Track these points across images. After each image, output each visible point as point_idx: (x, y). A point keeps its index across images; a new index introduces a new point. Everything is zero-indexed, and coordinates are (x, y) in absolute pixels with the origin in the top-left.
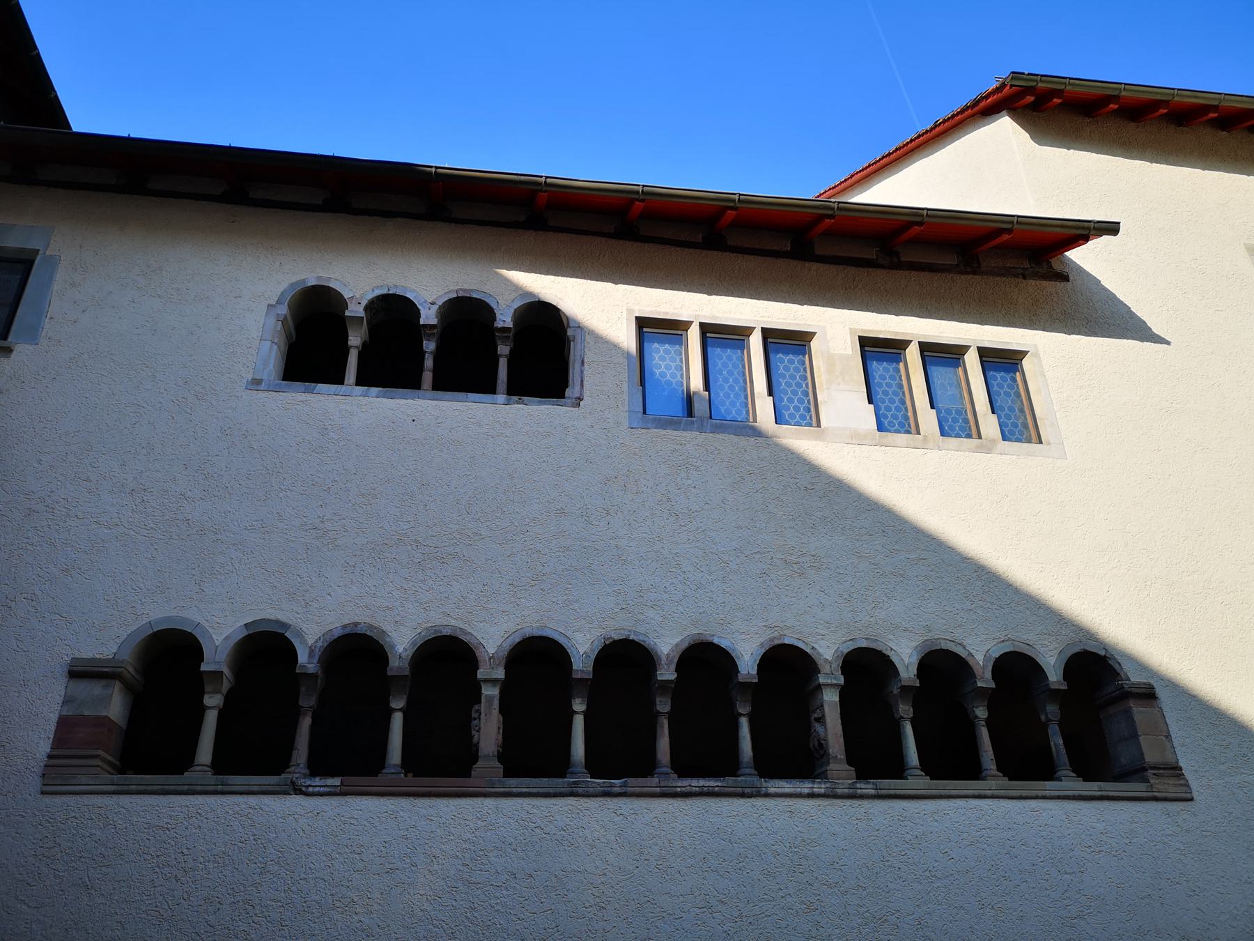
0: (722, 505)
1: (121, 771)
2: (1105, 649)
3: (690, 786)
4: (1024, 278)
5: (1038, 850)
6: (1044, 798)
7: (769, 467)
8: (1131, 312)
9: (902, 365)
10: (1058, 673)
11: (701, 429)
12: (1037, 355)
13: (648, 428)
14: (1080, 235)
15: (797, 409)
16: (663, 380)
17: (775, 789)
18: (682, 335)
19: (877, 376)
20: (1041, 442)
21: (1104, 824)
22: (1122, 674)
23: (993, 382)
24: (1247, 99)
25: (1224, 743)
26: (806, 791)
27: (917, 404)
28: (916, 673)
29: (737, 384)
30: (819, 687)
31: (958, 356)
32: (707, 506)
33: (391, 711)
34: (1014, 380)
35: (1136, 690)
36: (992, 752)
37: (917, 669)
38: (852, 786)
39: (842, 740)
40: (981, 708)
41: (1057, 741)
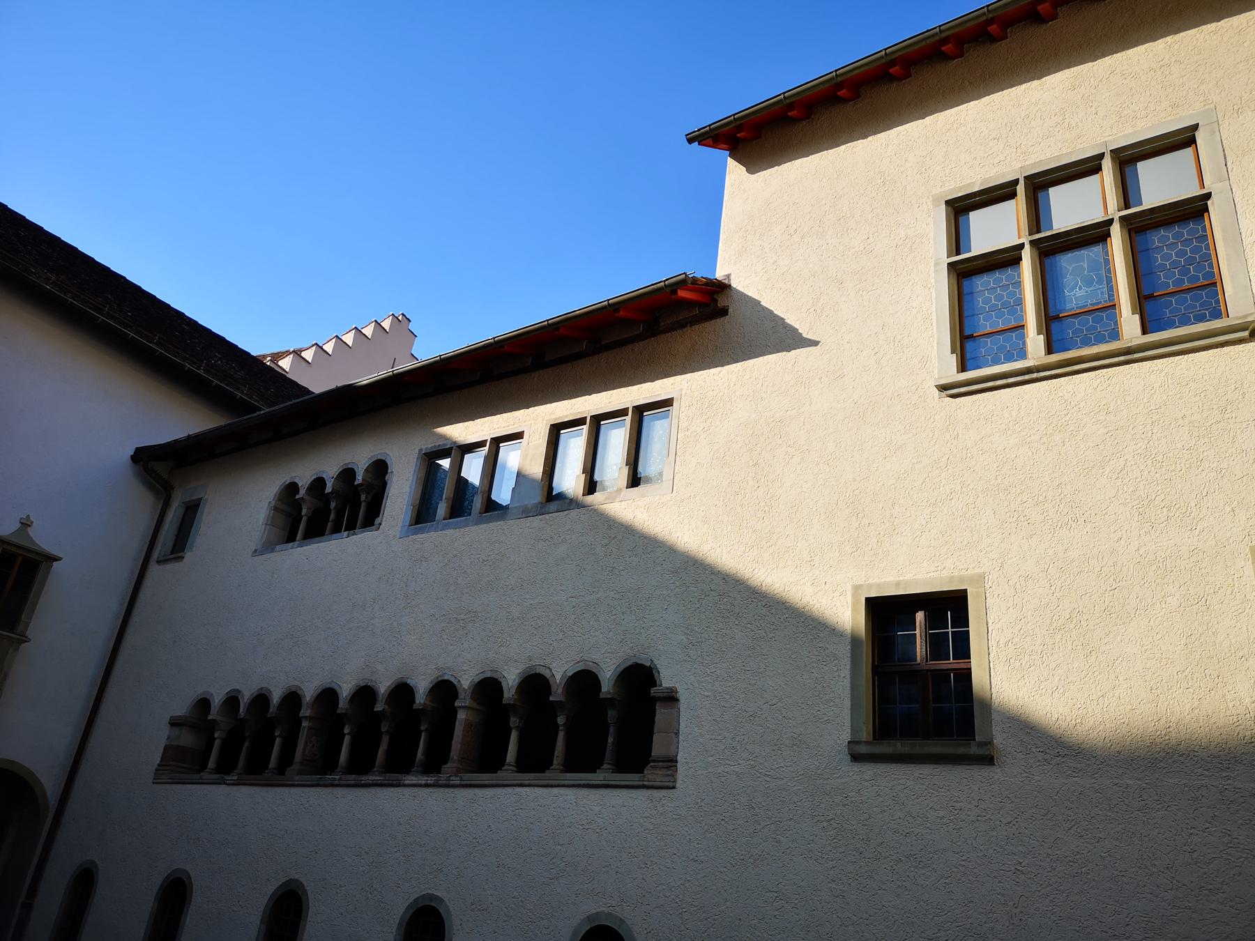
1: (518, 772)
26: (424, 782)
33: (344, 735)
35: (661, 695)
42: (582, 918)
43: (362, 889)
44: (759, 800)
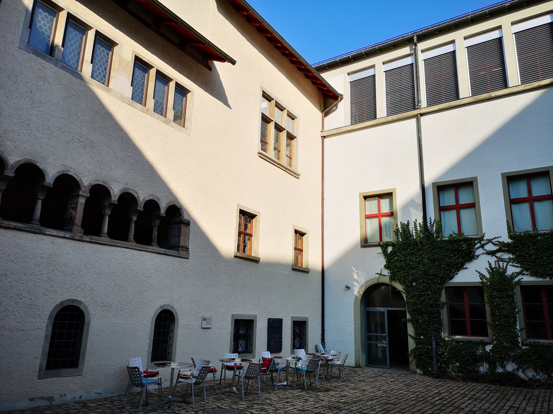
0: (57, 105)
2: (181, 206)
3: (10, 224)
4: (198, 62)
5: (139, 268)
6: (147, 251)
7: (82, 96)
8: (225, 92)
9: (111, 53)
10: (164, 210)
11: (56, 64)
12: (193, 94)
13: (29, 52)
14: (224, 59)
15: (100, 74)
16: (41, 30)
17: (49, 232)
18: (57, 13)
19: (136, 75)
20: (184, 127)
21: (162, 263)
22: (183, 215)
23: (39, 15)
24: (280, 37)
25: (202, 243)
26: (62, 235)
27: (148, 94)
28: (117, 199)
29: (77, 50)
30: (78, 196)
31: (168, 82)
32: (49, 102)
34: (144, 76)
36: (133, 233)
37: (118, 198)
38: (81, 237)
39: (81, 218)
40: (135, 217)
41: (155, 233)
42: (158, 307)
43: (12, 296)
44: (212, 266)
